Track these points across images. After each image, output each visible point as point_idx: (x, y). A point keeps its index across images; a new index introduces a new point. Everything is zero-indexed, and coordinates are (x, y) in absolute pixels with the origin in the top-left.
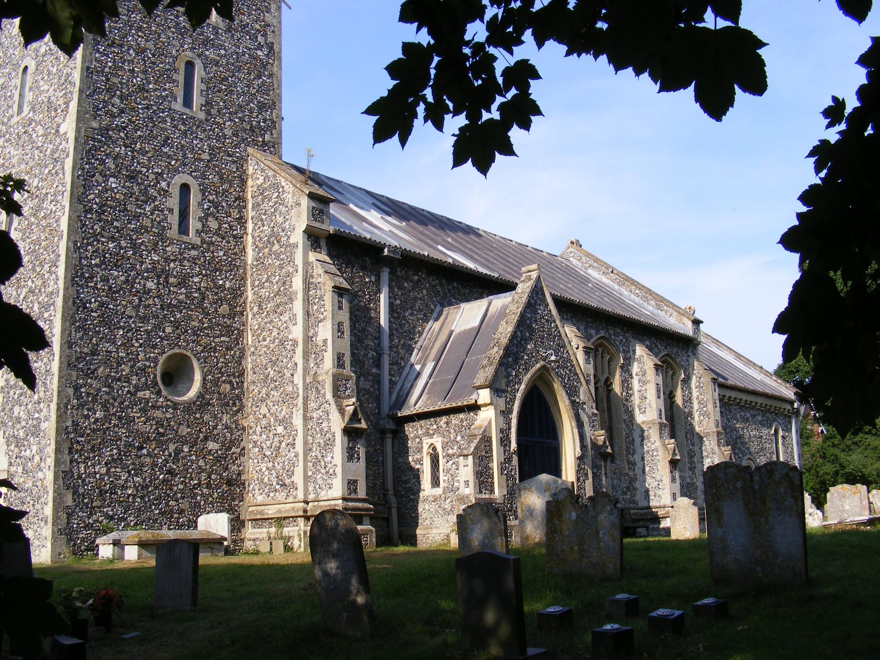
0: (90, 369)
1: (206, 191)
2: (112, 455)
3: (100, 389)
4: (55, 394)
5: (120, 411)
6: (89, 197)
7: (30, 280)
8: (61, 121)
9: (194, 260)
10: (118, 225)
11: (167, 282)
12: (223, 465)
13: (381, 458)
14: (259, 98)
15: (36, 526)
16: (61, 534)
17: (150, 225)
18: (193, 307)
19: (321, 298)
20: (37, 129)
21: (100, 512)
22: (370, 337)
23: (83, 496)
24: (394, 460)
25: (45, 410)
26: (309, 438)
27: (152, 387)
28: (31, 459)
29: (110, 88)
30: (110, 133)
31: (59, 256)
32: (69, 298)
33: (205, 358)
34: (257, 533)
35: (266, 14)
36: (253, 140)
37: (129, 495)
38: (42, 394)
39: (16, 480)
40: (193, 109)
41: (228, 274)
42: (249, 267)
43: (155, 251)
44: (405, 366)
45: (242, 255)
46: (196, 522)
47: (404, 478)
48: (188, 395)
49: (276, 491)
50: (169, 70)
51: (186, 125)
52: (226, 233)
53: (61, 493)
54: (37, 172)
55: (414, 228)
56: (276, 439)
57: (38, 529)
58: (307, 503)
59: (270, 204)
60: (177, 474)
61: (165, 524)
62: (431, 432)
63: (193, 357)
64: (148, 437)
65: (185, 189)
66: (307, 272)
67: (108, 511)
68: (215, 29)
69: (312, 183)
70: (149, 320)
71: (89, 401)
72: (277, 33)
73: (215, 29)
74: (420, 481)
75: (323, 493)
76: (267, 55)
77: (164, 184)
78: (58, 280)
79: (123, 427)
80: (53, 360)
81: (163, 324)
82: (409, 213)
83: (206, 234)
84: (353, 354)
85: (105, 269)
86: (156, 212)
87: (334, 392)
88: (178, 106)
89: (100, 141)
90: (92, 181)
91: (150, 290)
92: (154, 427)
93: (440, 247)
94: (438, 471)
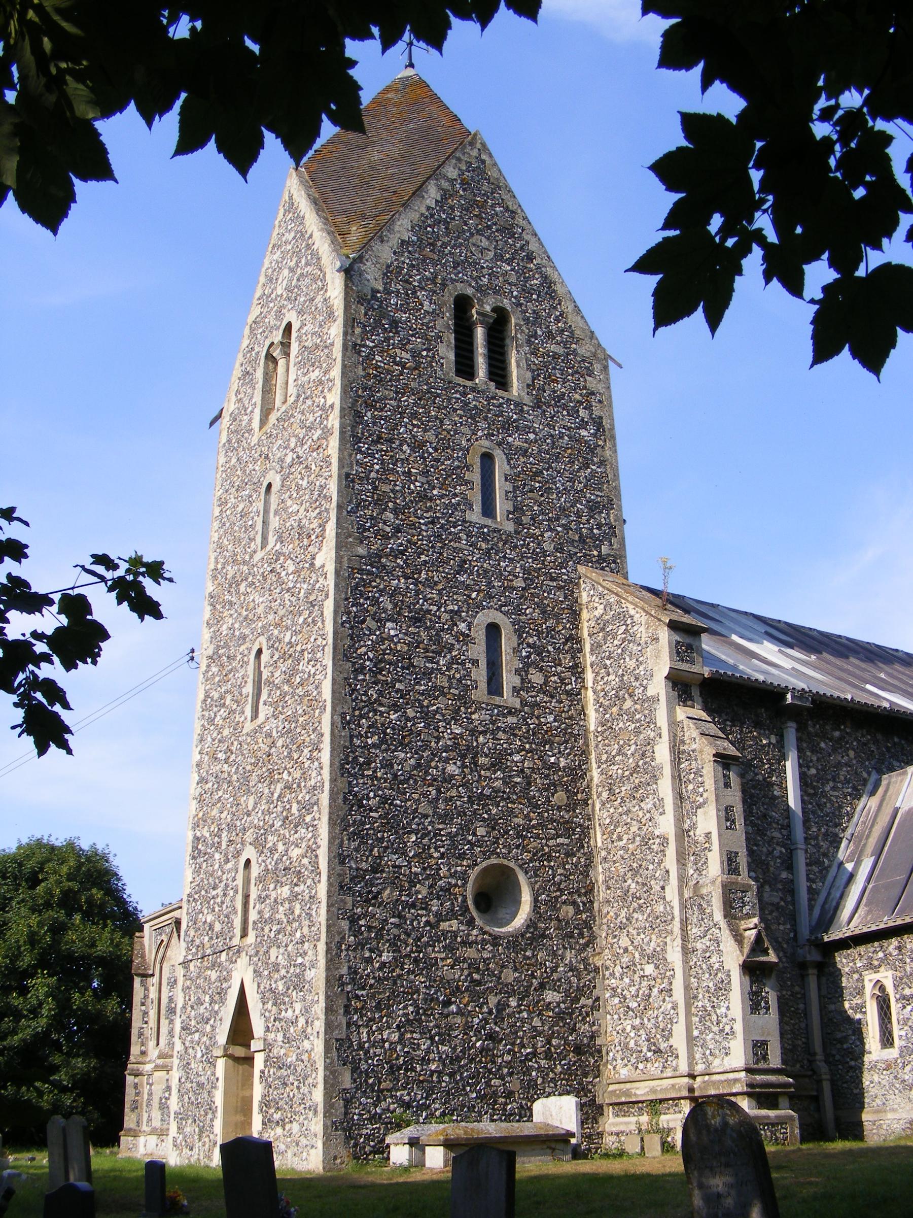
0: (371, 892)
1: (524, 632)
2: (407, 1014)
3: (386, 920)
4: (324, 929)
5: (417, 951)
6: (359, 652)
7: (286, 772)
8: (316, 550)
9: (511, 731)
10: (402, 687)
11: (476, 764)
12: (569, 1024)
13: (801, 1006)
14: (588, 495)
15: (302, 1118)
16: (336, 1129)
17: (447, 685)
18: (515, 797)
19: (698, 773)
20: (286, 565)
21: (391, 1097)
22: (774, 826)
23: (367, 1075)
24: (823, 1009)
25: (310, 953)
26: (693, 980)
27: (460, 915)
28: (294, 1022)
29: (378, 499)
30: (383, 560)
31: (322, 735)
32: (338, 793)
33: (536, 870)
34: (621, 1123)
35: (588, 378)
36: (585, 555)
37: (432, 1072)
38: (306, 930)
39: (276, 1052)
40: (496, 518)
41: (562, 748)
42: (591, 736)
43: (456, 720)
44: (830, 866)
45: (581, 719)
46: (530, 1110)
47: (839, 1035)
48: (513, 924)
49: (647, 1060)
50: (458, 467)
51: (489, 541)
52: (556, 688)
53: (336, 1071)
54: (289, 622)
55: (828, 662)
56: (645, 984)
57: (306, 1122)
58: (693, 1077)
59: (616, 642)
60: (502, 1039)
61: (486, 1113)
62: (876, 963)
63: (517, 869)
64: (458, 987)
65: (493, 630)
66: (675, 736)
67: (402, 1095)
68: (518, 405)
69: (673, 608)
70: (452, 819)
71: (371, 938)
72: (606, 402)
73: (518, 405)
74: (863, 1038)
75: (717, 1062)
76: (594, 435)
77: (462, 626)
78: (321, 768)
79: (421, 974)
80: (319, 881)
81: (472, 824)
82: (820, 642)
83: (528, 692)
84: (751, 853)
85: (386, 750)
86: (455, 666)
87: (725, 909)
88: (475, 516)
89: (370, 573)
90: (362, 629)
91: (452, 777)
92: (466, 972)
93: (869, 687)
94: (890, 1022)
